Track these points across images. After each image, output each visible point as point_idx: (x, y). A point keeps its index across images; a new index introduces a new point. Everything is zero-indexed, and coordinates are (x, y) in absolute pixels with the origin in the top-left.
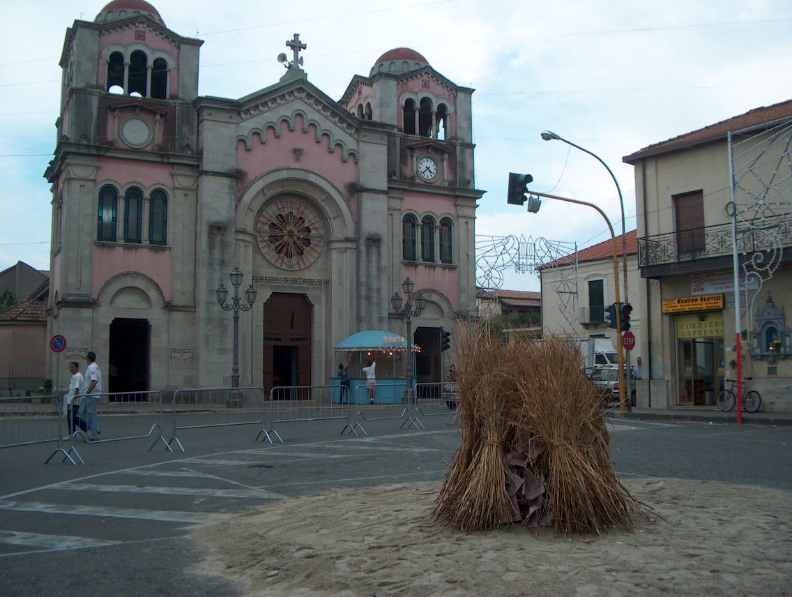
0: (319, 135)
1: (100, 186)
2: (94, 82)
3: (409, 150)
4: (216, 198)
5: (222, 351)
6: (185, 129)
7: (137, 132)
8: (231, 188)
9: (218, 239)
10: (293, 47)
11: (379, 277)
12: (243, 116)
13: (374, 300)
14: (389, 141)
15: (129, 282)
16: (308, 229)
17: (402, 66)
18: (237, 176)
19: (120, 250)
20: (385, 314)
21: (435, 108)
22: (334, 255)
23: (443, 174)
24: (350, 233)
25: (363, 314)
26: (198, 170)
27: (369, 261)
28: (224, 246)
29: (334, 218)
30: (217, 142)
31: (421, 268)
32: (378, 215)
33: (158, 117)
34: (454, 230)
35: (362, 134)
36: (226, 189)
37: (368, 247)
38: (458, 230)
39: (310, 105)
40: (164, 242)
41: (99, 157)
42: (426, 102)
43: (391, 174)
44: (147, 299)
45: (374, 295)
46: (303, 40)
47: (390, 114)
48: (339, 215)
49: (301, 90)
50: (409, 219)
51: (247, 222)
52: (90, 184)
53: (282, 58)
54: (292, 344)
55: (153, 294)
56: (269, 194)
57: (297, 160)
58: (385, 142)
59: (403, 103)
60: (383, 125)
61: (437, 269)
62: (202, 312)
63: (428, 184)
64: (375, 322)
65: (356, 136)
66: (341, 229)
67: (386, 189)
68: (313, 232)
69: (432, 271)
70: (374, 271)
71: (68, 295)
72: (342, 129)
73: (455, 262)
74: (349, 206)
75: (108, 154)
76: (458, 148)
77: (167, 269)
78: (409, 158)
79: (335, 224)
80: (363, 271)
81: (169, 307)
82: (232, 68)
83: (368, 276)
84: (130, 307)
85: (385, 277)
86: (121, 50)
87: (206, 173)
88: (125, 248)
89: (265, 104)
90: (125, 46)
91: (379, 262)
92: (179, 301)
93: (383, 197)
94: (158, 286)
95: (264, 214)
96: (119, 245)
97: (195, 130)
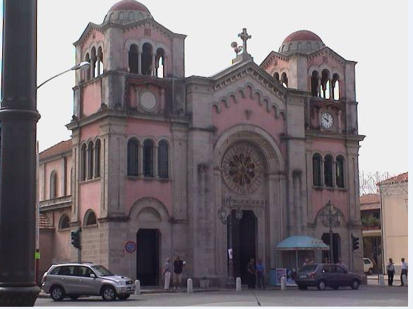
1: (128, 139)
2: (122, 67)
5: (207, 251)
6: (178, 98)
9: (203, 174)
12: (216, 88)
13: (299, 214)
15: (154, 205)
16: (253, 166)
17: (305, 45)
18: (212, 130)
19: (141, 182)
20: (305, 224)
21: (154, 52)
22: (271, 183)
24: (281, 168)
25: (292, 224)
26: (189, 128)
27: (295, 188)
28: (207, 178)
30: (200, 105)
31: (324, 191)
32: (299, 156)
38: (348, 165)
40: (167, 176)
42: (147, 47)
44: (157, 214)
45: (298, 212)
48: (274, 155)
50: (316, 158)
51: (218, 162)
53: (234, 45)
57: (248, 118)
59: (311, 74)
61: (335, 192)
63: (328, 132)
64: (299, 230)
66: (275, 165)
67: (304, 137)
68: (256, 167)
70: (298, 195)
71: (112, 213)
73: (346, 188)
74: (280, 148)
75: (135, 117)
76: (347, 106)
77: (167, 194)
78: (316, 114)
79: (271, 162)
81: (172, 221)
82: (205, 58)
83: (295, 198)
84: (147, 221)
85: (304, 199)
86: (137, 43)
87: (194, 129)
88: (145, 180)
90: (139, 40)
91: (300, 188)
92: (179, 216)
93: (302, 143)
94: (165, 207)
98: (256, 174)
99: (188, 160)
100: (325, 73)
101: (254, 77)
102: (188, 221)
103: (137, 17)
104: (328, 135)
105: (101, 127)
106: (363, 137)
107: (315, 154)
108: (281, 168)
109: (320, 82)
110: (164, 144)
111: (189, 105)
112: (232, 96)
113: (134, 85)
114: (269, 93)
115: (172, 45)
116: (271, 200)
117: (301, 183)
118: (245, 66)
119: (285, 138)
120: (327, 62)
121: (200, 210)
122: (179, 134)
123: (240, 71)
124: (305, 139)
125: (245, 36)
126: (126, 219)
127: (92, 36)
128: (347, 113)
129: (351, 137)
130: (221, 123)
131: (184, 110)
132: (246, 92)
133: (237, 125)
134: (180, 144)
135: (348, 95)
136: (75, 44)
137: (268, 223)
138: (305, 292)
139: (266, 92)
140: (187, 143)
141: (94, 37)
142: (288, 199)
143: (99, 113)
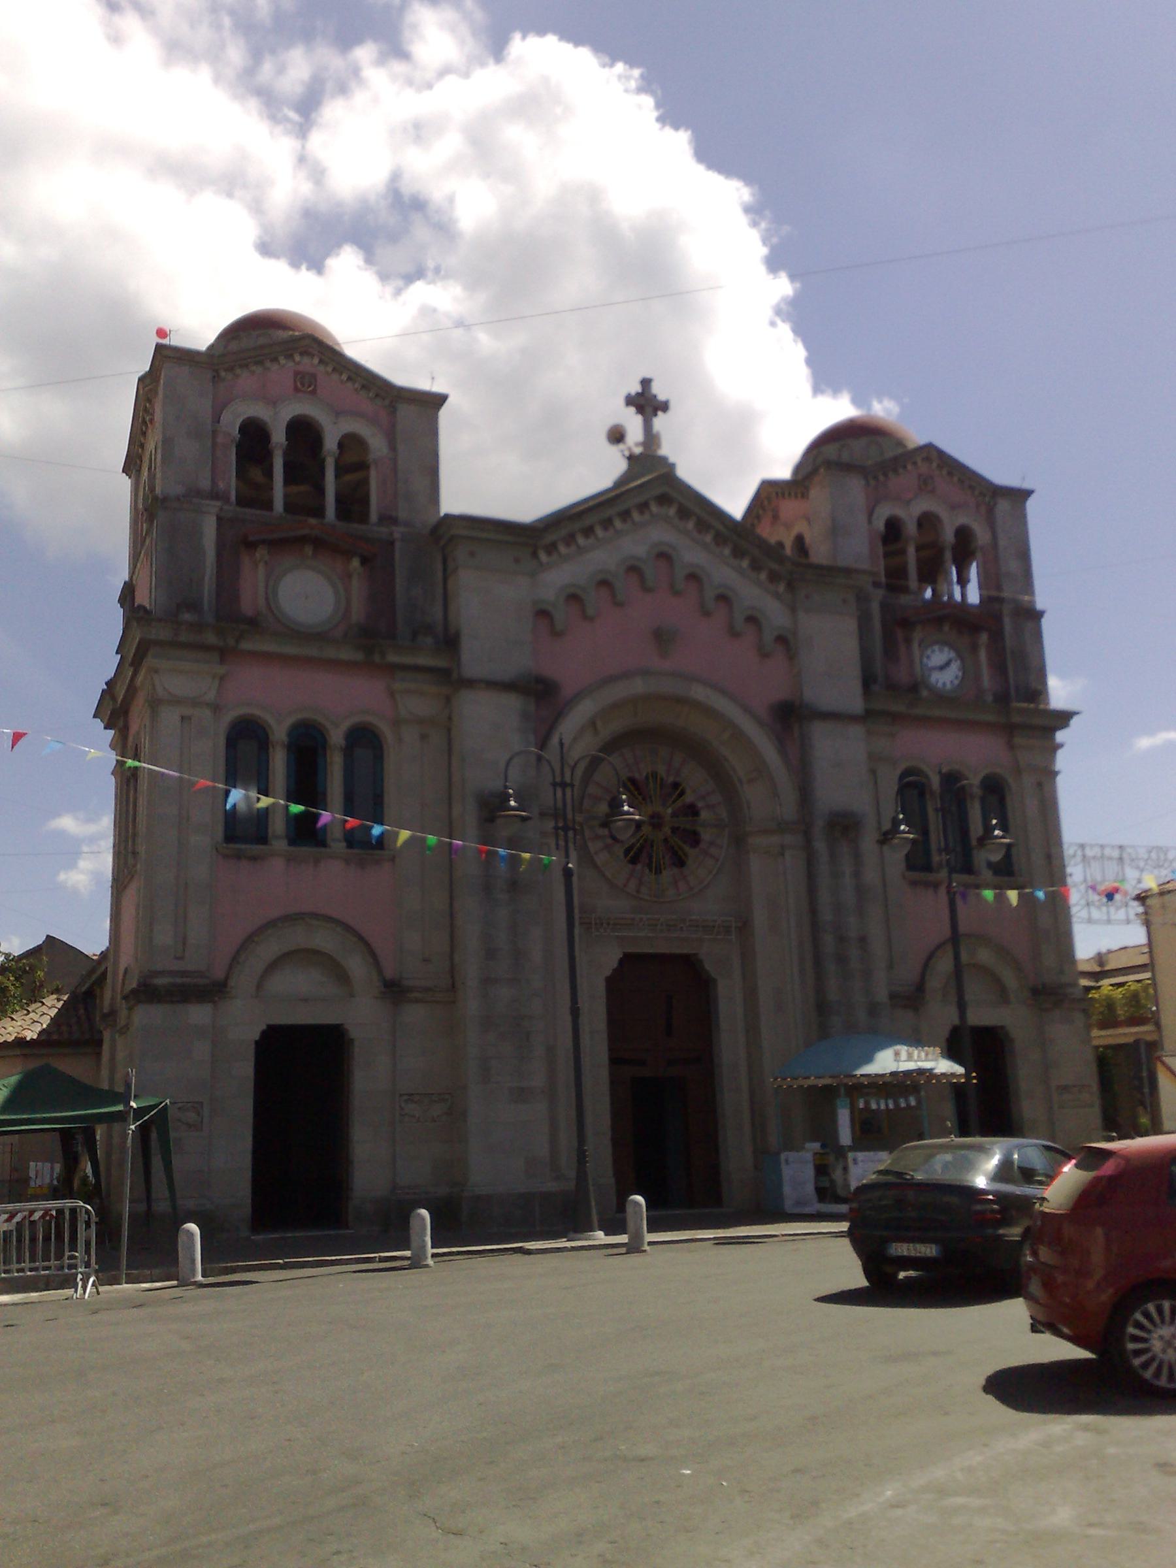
1: (228, 717)
12: (543, 557)
15: (324, 940)
19: (277, 865)
20: (882, 995)
22: (756, 864)
26: (451, 680)
30: (489, 613)
32: (848, 768)
44: (341, 976)
50: (912, 787)
59: (880, 525)
63: (942, 698)
79: (754, 796)
81: (394, 991)
84: (300, 998)
86: (900, 512)
91: (857, 874)
93: (856, 731)
98: (706, 835)
100: (964, 535)
101: (647, 516)
104: (951, 712)
106: (1063, 718)
107: (907, 772)
108: (788, 807)
109: (948, 555)
110: (364, 739)
112: (604, 583)
115: (393, 425)
116: (760, 918)
117: (857, 856)
119: (790, 717)
120: (933, 491)
121: (490, 954)
122: (419, 702)
124: (868, 716)
125: (646, 403)
126: (210, 991)
128: (1009, 642)
129: (1025, 719)
133: (626, 675)
134: (424, 737)
137: (751, 994)
138: (325, 794)
140: (446, 726)
142: (813, 911)
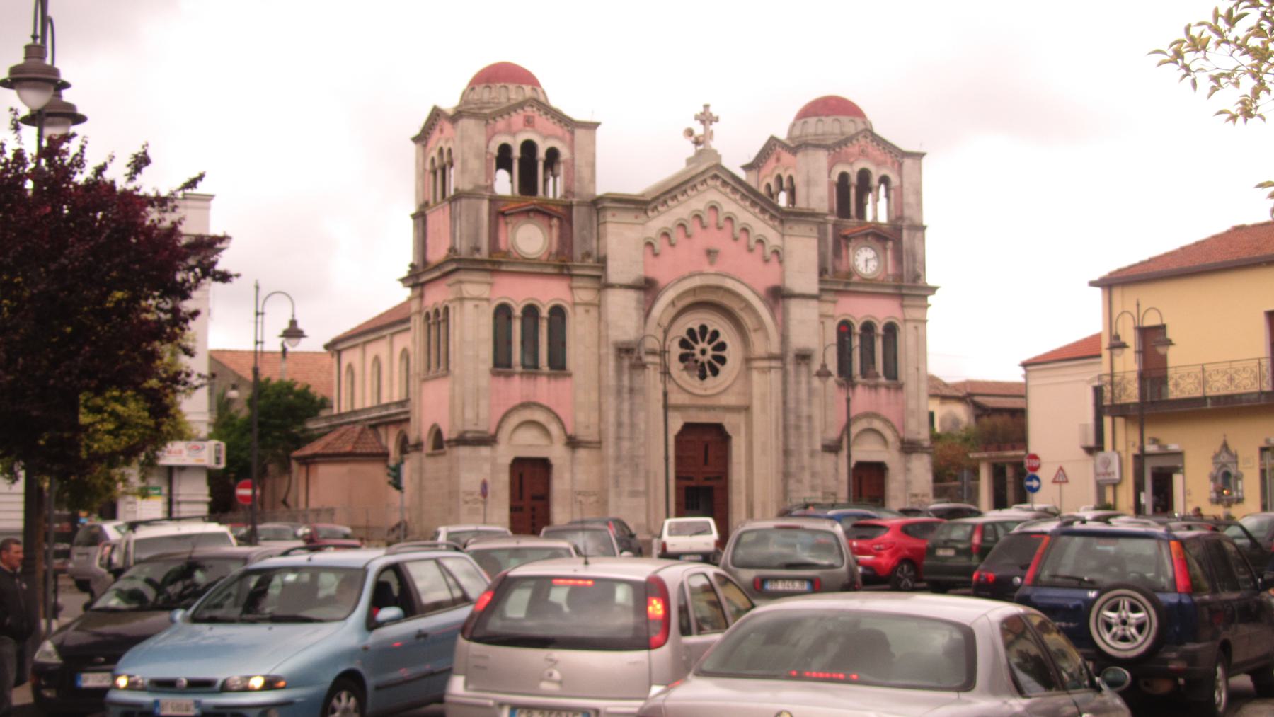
0: (737, 229)
3: (842, 241)
4: (623, 314)
5: (634, 494)
7: (531, 239)
8: (638, 301)
10: (703, 122)
11: (810, 403)
14: (819, 232)
15: (539, 416)
19: (517, 378)
20: (818, 446)
22: (755, 376)
23: (886, 267)
24: (775, 348)
25: (792, 447)
26: (604, 285)
27: (798, 383)
29: (755, 330)
30: (623, 246)
32: (810, 327)
33: (555, 221)
34: (901, 337)
35: (787, 226)
36: (633, 304)
37: (798, 364)
38: (906, 338)
39: (725, 194)
40: (563, 367)
41: (493, 272)
43: (822, 271)
44: (885, 441)
45: (804, 424)
46: (714, 111)
47: (819, 196)
48: (761, 326)
49: (715, 177)
50: (845, 329)
52: (485, 303)
53: (690, 132)
54: (708, 483)
55: (554, 428)
56: (680, 305)
57: (711, 263)
58: (815, 234)
59: (835, 178)
60: (813, 214)
62: (610, 450)
65: (780, 228)
69: (873, 394)
71: (466, 432)
72: (764, 221)
73: (902, 377)
75: (504, 268)
79: (756, 338)
80: (791, 395)
81: (573, 443)
84: (528, 443)
85: (816, 401)
87: (612, 286)
89: (675, 198)
92: (583, 434)
93: (814, 303)
95: (484, 254)
96: (542, 374)
97: (595, 232)
99: (601, 339)
102: (600, 442)
103: (515, 94)
105: (450, 285)
106: (933, 290)
110: (558, 313)
111: (602, 242)
112: (666, 235)
113: (503, 214)
114: (751, 217)
118: (707, 171)
122: (585, 295)
123: (706, 176)
127: (438, 128)
129: (910, 287)
130: (661, 272)
131: (595, 253)
132: (708, 218)
135: (907, 212)
136: (416, 140)
139: (746, 215)
141: (442, 131)
143: (448, 261)
